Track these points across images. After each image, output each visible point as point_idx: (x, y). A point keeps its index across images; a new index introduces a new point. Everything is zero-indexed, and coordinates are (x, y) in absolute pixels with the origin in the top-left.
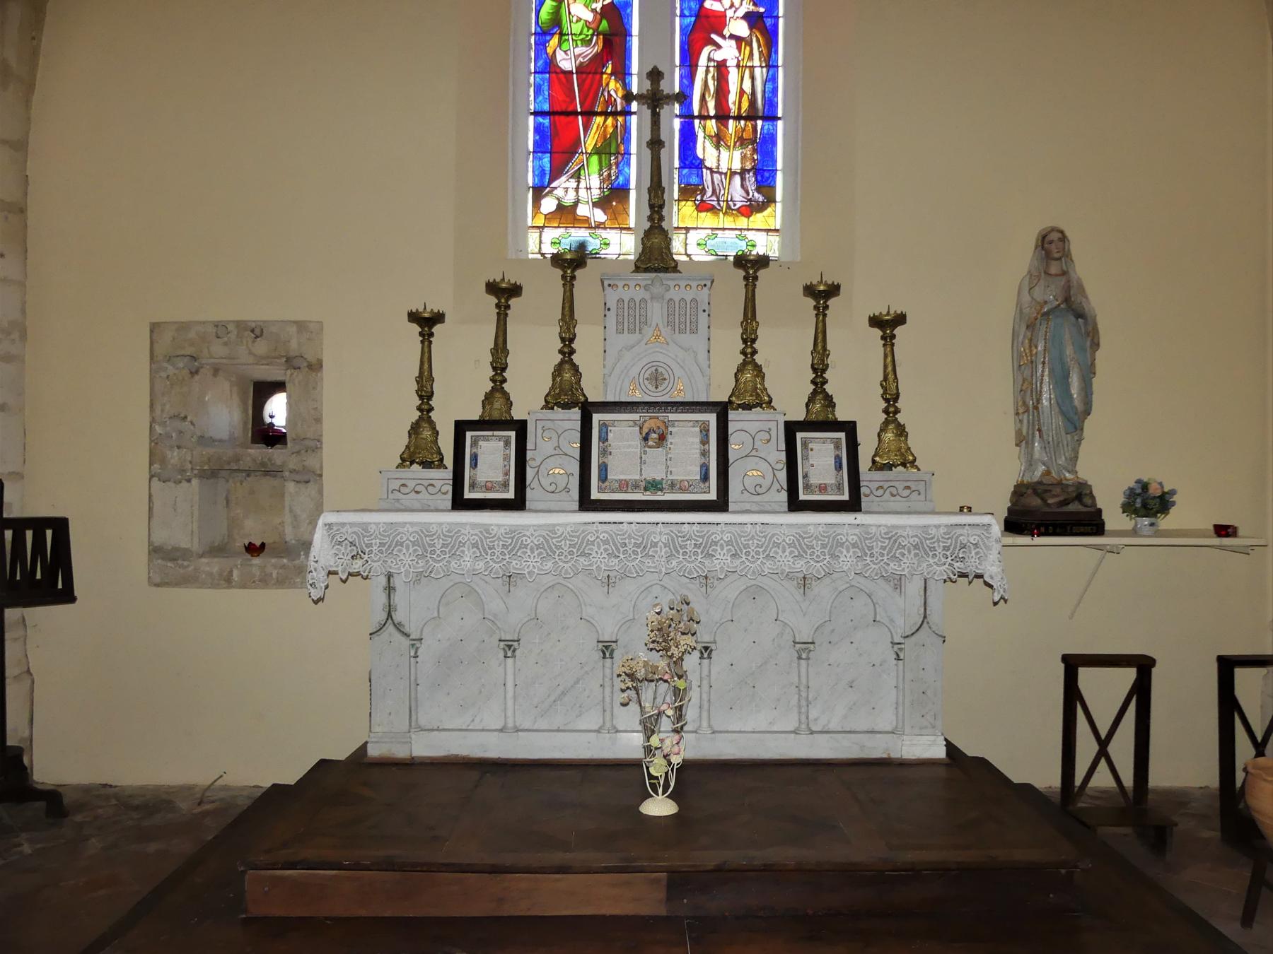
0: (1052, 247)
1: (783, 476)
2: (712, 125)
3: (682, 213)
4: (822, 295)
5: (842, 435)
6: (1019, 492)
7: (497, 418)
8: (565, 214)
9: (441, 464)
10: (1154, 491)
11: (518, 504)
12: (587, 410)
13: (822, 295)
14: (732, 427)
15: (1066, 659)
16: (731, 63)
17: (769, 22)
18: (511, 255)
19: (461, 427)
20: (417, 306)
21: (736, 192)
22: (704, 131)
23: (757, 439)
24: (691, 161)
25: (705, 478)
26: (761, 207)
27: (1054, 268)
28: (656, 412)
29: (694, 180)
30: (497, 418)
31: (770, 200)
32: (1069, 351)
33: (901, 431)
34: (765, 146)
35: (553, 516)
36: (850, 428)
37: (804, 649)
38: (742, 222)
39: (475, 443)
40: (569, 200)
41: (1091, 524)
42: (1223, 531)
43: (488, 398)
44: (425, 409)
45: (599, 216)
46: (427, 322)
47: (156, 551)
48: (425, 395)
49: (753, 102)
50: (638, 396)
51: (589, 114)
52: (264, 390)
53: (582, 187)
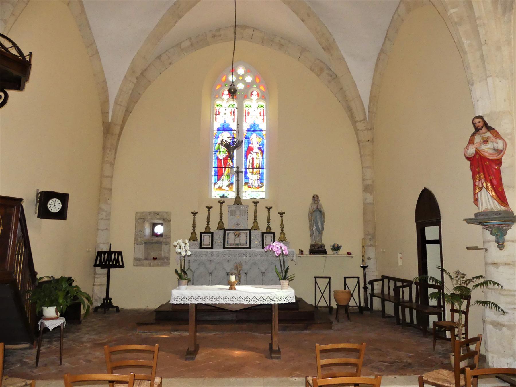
0: (315, 198)
1: (261, 243)
2: (251, 170)
3: (244, 188)
4: (269, 209)
5: (272, 235)
6: (312, 246)
7: (208, 232)
8: (220, 188)
9: (197, 240)
10: (336, 245)
11: (212, 247)
12: (225, 230)
13: (269, 209)
14: (251, 234)
15: (315, 277)
16: (255, 158)
17: (262, 149)
18: (209, 197)
19: (201, 234)
20: (193, 211)
21: (256, 184)
22: (249, 171)
23: (256, 237)
24: (247, 178)
25: (247, 243)
26: (261, 187)
27: (316, 202)
28: (237, 231)
29: (247, 181)
30: (208, 232)
31: (263, 186)
32: (318, 219)
33: (284, 234)
34: (261, 174)
35: (218, 249)
36: (274, 234)
37: (263, 274)
38: (257, 190)
39: (204, 236)
40: (221, 186)
41: (325, 252)
42: (348, 253)
43: (206, 228)
44: (194, 230)
45: (227, 189)
46: (194, 214)
47: (135, 259)
48: (194, 227)
49: (259, 166)
50: (234, 228)
51: (225, 168)
52: (154, 225)
53: (224, 182)
